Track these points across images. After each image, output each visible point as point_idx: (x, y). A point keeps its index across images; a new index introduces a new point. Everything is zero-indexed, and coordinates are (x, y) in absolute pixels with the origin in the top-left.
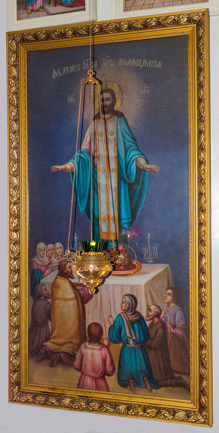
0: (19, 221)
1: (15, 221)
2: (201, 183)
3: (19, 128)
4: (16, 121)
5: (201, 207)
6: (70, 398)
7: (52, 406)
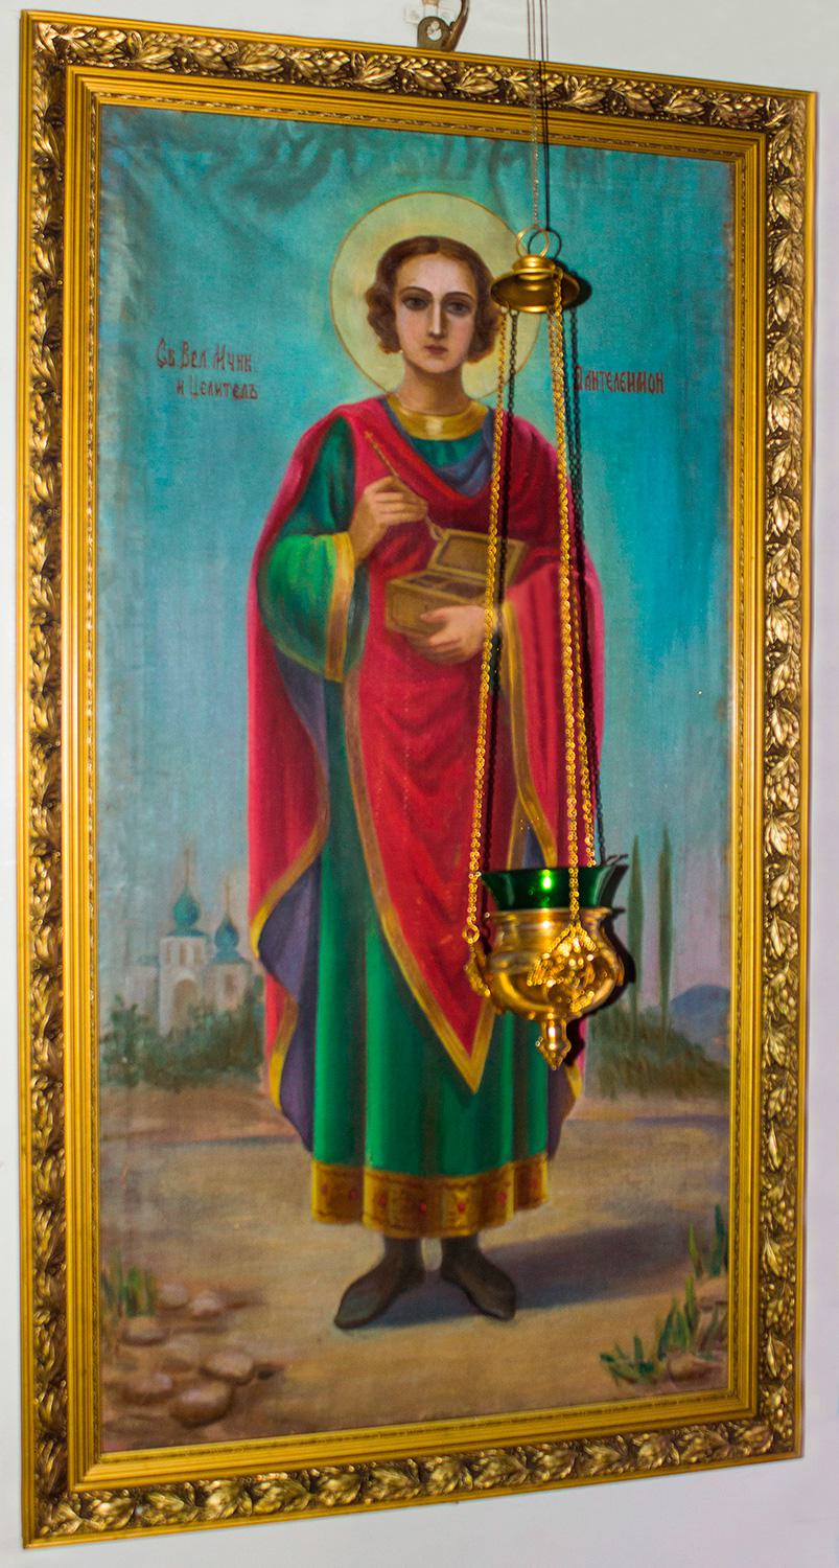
0: (768, 682)
1: (781, 897)
2: (48, 382)
3: (764, 829)
4: (776, 857)
5: (48, 525)
6: (573, 109)
7: (640, 82)
